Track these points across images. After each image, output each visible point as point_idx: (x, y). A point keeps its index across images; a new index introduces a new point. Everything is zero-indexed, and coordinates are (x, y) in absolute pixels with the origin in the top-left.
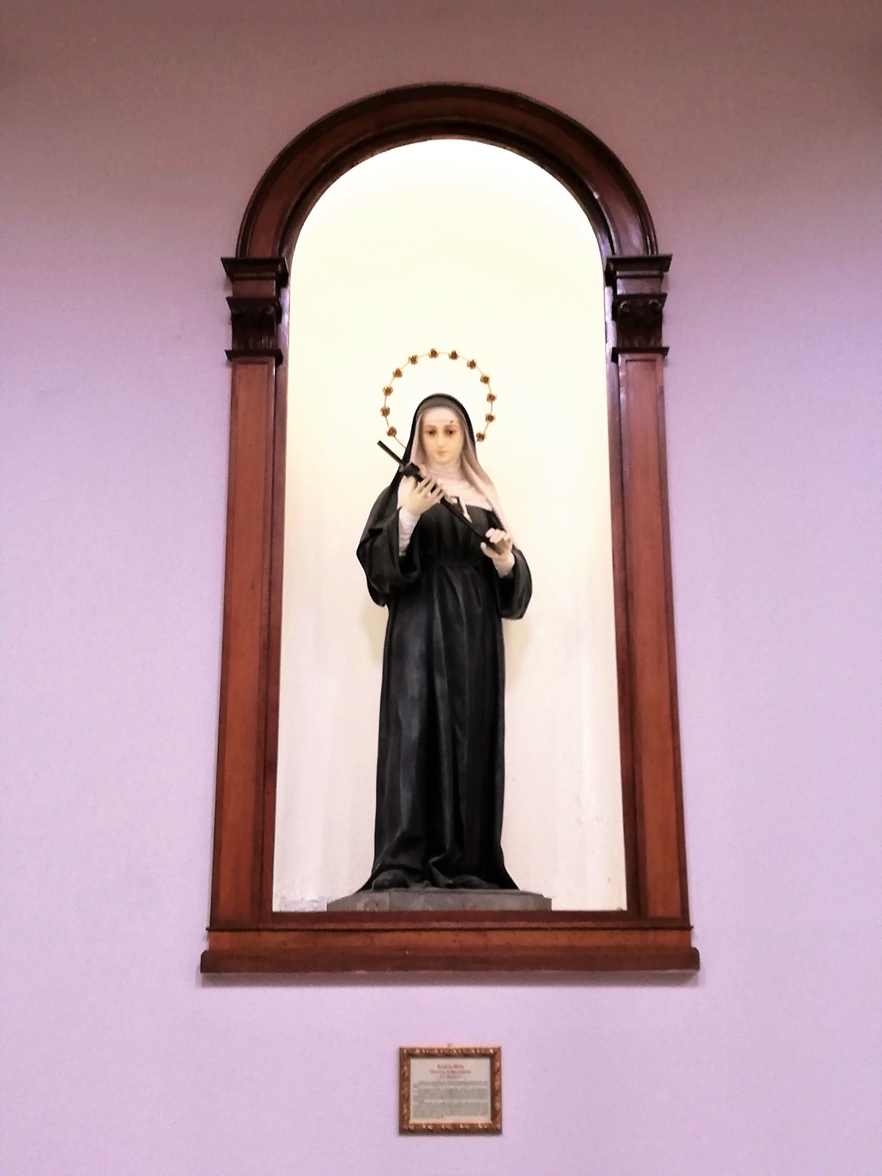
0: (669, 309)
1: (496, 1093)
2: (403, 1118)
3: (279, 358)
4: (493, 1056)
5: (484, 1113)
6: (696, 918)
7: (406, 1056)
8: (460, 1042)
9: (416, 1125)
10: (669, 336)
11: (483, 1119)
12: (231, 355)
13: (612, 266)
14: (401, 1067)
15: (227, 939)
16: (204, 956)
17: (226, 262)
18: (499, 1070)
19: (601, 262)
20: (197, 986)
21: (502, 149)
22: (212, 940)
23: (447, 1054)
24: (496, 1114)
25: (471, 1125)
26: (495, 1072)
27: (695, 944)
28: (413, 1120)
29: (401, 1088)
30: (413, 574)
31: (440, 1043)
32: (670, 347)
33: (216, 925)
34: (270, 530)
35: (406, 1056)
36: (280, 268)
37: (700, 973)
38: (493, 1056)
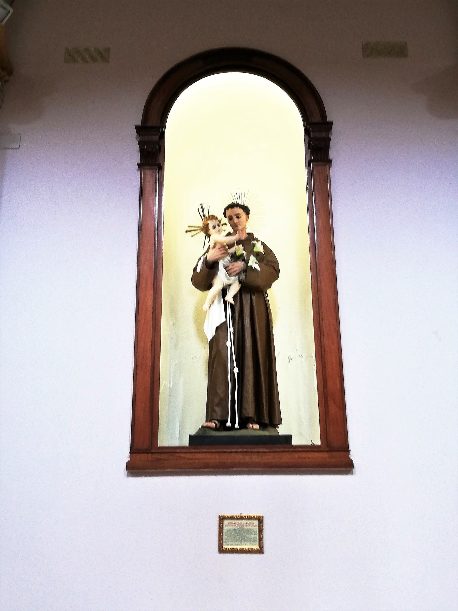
0: (332, 144)
1: (261, 531)
3: (161, 168)
5: (254, 540)
6: (352, 446)
9: (226, 549)
10: (332, 155)
11: (256, 547)
12: (140, 166)
13: (308, 127)
16: (128, 463)
17: (137, 127)
21: (274, 332)
22: (131, 457)
23: (241, 518)
24: (261, 540)
25: (252, 549)
27: (351, 457)
28: (225, 547)
31: (236, 513)
32: (333, 160)
33: (134, 451)
34: (154, 328)
36: (161, 130)
37: (354, 470)
38: (260, 520)
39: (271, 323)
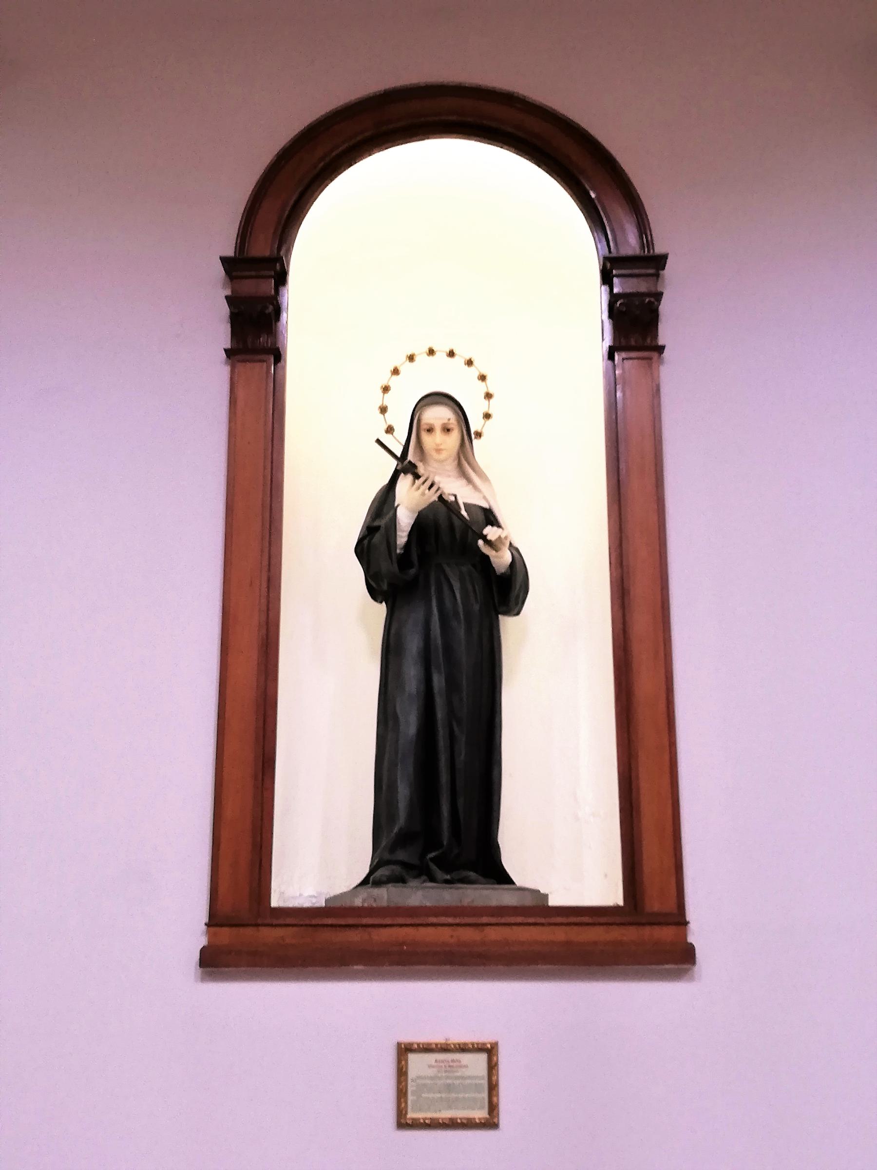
0: (665, 308)
1: (493, 1087)
2: (401, 1112)
3: (278, 356)
4: (490, 1051)
5: (482, 1108)
6: (692, 913)
7: (404, 1050)
8: (457, 1037)
9: (413, 1119)
10: (666, 334)
11: (480, 1114)
12: (230, 353)
13: (608, 265)
14: (399, 1061)
15: (226, 935)
16: (203, 951)
17: (224, 260)
18: (497, 1064)
19: (598, 261)
20: (196, 981)
22: (210, 935)
23: (445, 1049)
24: (493, 1108)
25: (469, 1119)
26: (492, 1067)
27: (691, 939)
28: (411, 1115)
29: (399, 1082)
30: (411, 571)
31: (438, 1038)
32: (667, 346)
33: (215, 920)
35: (404, 1050)
36: (278, 266)
38: (490, 1051)
39: (454, 410)
